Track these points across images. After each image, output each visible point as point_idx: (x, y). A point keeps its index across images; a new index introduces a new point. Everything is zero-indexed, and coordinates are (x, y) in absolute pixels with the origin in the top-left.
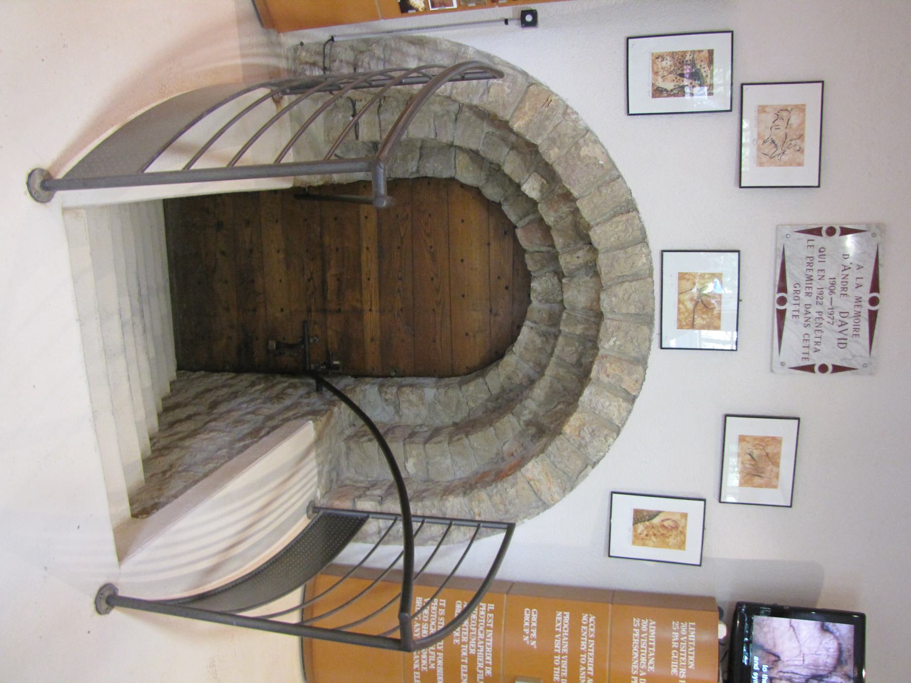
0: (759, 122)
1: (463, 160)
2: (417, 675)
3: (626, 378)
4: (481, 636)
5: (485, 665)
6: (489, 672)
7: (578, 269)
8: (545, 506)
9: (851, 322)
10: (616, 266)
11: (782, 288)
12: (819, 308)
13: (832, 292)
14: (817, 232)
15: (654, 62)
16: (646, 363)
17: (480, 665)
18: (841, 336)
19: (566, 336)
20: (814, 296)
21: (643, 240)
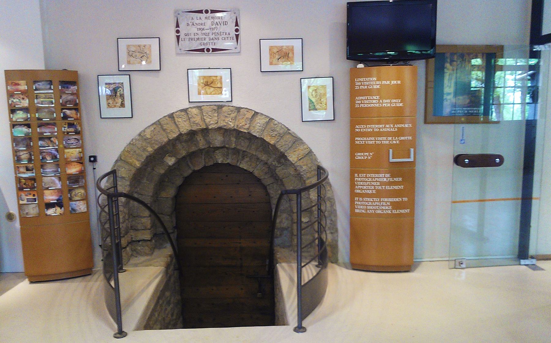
0: (133, 64)
1: (164, 194)
2: (394, 212)
3: (247, 116)
4: (370, 180)
5: (385, 177)
6: (388, 175)
7: (206, 140)
8: (310, 152)
9: (216, 21)
10: (197, 122)
11: (202, 50)
12: (210, 34)
13: (203, 29)
14: (178, 37)
15: (111, 107)
16: (239, 108)
17: (385, 180)
18: (222, 24)
19: (237, 145)
20: (205, 37)
21: (185, 110)
